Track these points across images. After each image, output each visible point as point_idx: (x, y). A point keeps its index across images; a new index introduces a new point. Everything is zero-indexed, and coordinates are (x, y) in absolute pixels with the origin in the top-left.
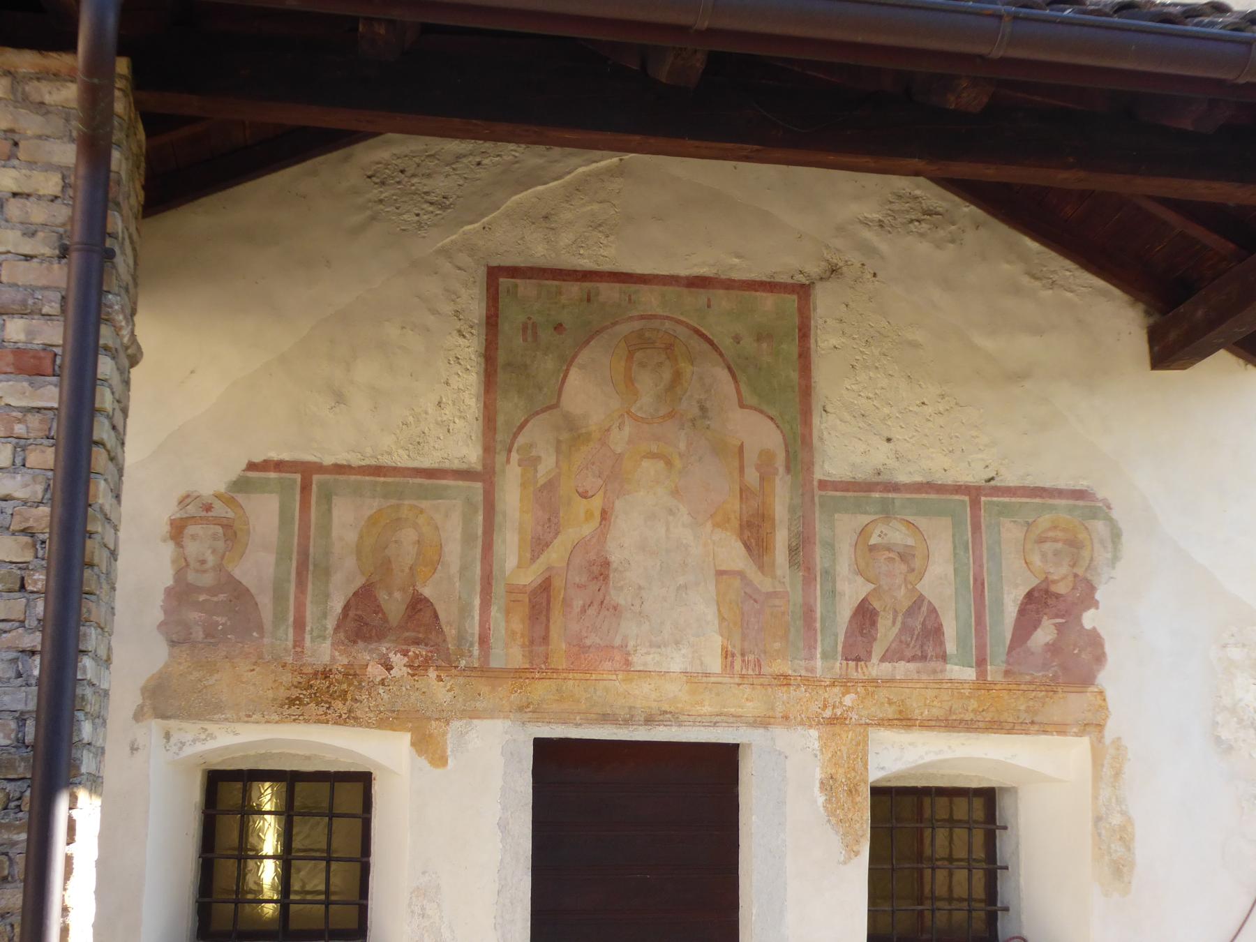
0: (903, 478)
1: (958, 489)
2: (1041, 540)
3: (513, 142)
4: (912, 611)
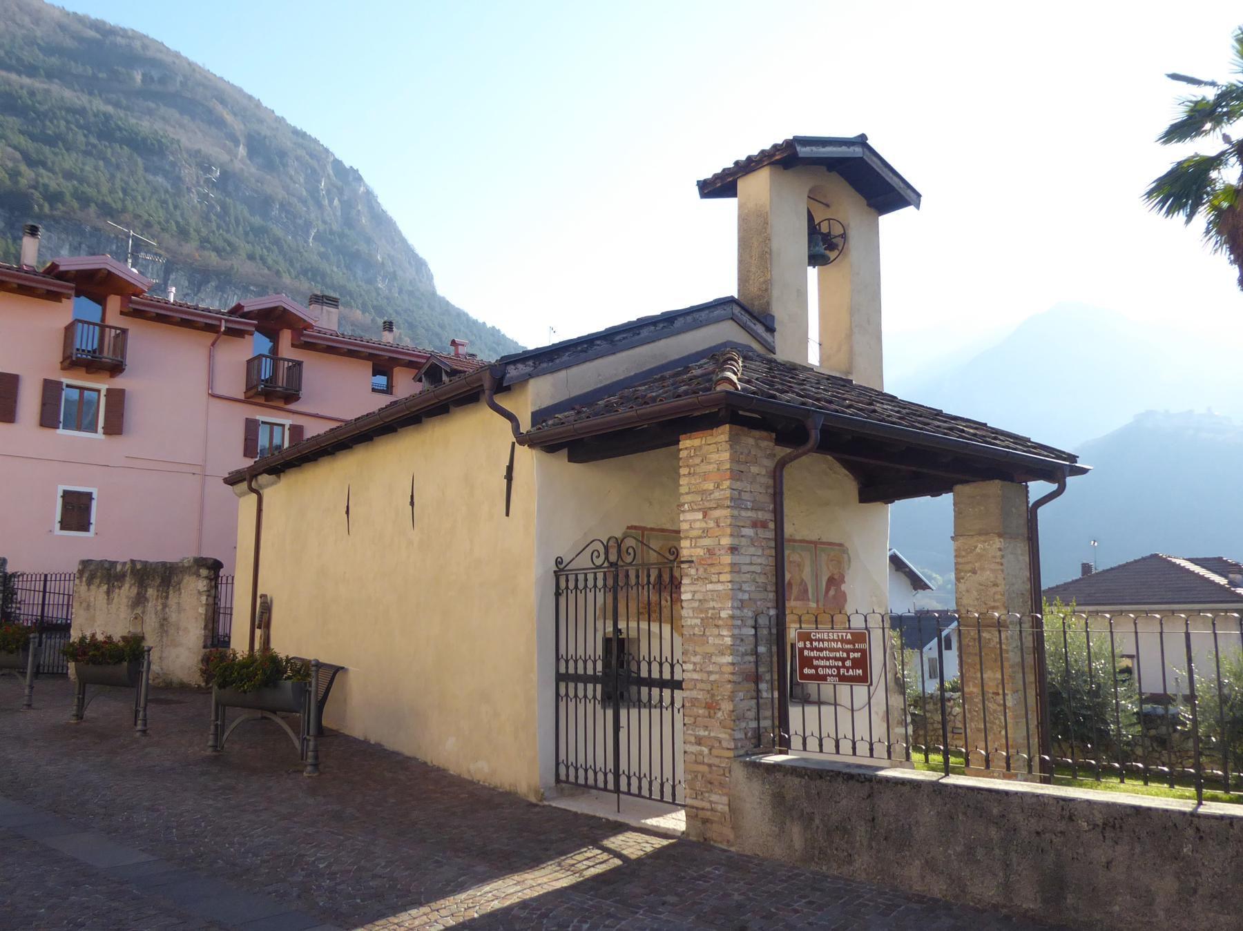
0: (798, 537)
1: (811, 542)
2: (832, 560)
3: (287, 124)
4: (801, 583)
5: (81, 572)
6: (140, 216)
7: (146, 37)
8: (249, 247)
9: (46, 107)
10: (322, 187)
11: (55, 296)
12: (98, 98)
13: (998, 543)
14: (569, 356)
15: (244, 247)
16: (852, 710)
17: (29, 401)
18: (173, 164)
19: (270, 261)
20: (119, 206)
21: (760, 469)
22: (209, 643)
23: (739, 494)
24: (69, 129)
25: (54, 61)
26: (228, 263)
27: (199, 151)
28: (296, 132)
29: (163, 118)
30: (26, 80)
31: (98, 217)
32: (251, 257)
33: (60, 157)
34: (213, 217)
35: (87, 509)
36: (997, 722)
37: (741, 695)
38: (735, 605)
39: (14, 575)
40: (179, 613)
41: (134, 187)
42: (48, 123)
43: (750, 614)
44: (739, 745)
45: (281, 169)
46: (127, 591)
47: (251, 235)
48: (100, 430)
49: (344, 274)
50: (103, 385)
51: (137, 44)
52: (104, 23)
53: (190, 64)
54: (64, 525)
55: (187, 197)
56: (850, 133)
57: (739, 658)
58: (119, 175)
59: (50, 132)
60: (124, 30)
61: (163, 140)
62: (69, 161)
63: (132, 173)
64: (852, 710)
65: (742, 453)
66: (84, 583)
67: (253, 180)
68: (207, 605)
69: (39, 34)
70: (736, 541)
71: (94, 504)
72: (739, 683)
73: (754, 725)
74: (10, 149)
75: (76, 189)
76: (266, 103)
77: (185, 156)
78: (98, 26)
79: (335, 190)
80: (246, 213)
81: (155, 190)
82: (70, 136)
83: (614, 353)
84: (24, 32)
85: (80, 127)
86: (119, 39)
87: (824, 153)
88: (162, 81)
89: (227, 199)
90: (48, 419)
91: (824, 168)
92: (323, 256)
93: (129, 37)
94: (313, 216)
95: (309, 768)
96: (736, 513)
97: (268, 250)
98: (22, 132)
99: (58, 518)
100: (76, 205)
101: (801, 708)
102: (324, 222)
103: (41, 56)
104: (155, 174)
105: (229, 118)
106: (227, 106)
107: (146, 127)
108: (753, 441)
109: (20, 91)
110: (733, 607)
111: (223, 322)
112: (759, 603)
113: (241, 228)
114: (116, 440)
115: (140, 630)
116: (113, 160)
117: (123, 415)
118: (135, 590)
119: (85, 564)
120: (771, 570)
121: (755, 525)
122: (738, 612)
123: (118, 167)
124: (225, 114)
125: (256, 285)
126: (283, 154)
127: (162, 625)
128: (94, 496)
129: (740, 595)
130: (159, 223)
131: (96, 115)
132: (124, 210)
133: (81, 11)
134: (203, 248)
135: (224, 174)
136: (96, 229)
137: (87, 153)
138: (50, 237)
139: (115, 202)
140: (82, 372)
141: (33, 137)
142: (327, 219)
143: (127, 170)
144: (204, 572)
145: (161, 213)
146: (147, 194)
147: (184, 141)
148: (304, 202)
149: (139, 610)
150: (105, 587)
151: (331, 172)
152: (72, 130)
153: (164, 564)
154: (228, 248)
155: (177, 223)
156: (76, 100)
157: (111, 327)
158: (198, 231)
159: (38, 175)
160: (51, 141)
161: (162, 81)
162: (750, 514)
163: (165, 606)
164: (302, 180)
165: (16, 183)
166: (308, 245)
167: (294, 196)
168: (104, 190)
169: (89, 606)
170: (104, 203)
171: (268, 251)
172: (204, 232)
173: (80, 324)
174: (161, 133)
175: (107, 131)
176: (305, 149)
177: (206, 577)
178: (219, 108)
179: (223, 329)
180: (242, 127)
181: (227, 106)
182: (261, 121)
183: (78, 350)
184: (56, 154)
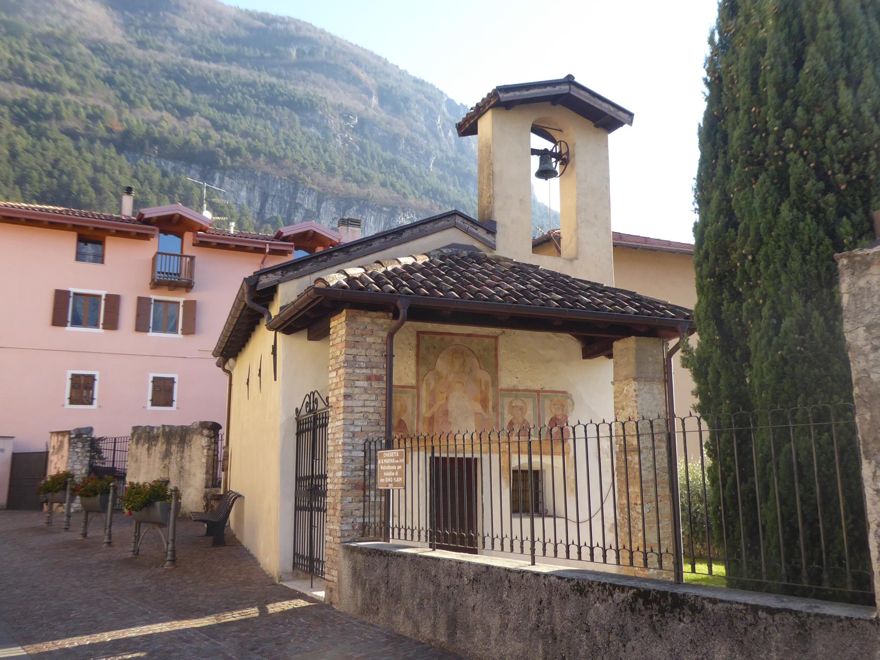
5: (133, 435)
6: (297, 160)
7: (299, 21)
8: (382, 177)
9: (228, 84)
10: (439, 122)
11: (145, 237)
12: (265, 72)
13: (634, 385)
14: (311, 265)
15: (378, 177)
16: (578, 523)
17: (128, 313)
18: (322, 117)
19: (398, 186)
20: (282, 154)
21: (376, 340)
22: (210, 484)
23: (354, 357)
24: (244, 98)
25: (233, 48)
26: (366, 191)
27: (341, 105)
28: (416, 81)
29: (314, 83)
30: (213, 66)
31: (266, 164)
32: (383, 185)
33: (238, 121)
34: (354, 156)
35: (170, 391)
36: (636, 526)
37: (350, 499)
38: (347, 435)
39: (100, 439)
40: (190, 463)
41: (294, 138)
42: (229, 96)
43: (361, 442)
44: (346, 534)
45: (406, 112)
46: (160, 448)
47: (384, 167)
48: (180, 332)
49: (459, 191)
50: (180, 298)
51: (293, 27)
52: (267, 14)
53: (332, 37)
54: (155, 403)
55: (334, 142)
56: (561, 76)
57: (349, 473)
58: (282, 130)
59: (231, 103)
60: (283, 18)
61: (314, 100)
62: (245, 123)
63: (292, 127)
64: (578, 523)
65: (357, 329)
66: (134, 444)
67: (384, 123)
68: (208, 456)
69: (221, 29)
70: (349, 391)
71: (176, 386)
72: (348, 491)
73: (361, 520)
74: (202, 120)
75: (249, 144)
76: (392, 60)
77: (330, 109)
78: (265, 18)
79: (449, 124)
80: (379, 150)
81: (309, 139)
82: (245, 105)
83: (350, 261)
84: (211, 29)
85: (252, 96)
86: (279, 26)
87: (528, 95)
88: (311, 53)
89: (365, 140)
90: (141, 326)
91: (548, 104)
92: (442, 178)
93: (286, 23)
94: (432, 147)
95: (168, 563)
96: (350, 371)
97: (398, 177)
98: (211, 105)
99: (150, 397)
100: (250, 156)
101: (519, 520)
102: (442, 151)
103: (223, 46)
104: (309, 127)
105: (363, 76)
106: (361, 67)
107: (300, 90)
108: (365, 320)
109: (208, 75)
110: (344, 437)
111: (268, 245)
112: (370, 434)
113: (376, 162)
114: (190, 338)
115: (166, 476)
116: (278, 119)
117: (195, 319)
118: (164, 447)
119: (135, 429)
120: (382, 410)
121: (369, 378)
122: (349, 441)
123: (281, 124)
124: (360, 73)
125: (387, 207)
126: (406, 100)
127: (180, 472)
128: (176, 380)
129: (352, 429)
130: (312, 164)
131: (263, 86)
132: (286, 157)
133: (250, 8)
134: (345, 180)
135: (362, 121)
136: (265, 174)
137: (258, 116)
138: (232, 183)
139: (279, 152)
140: (165, 290)
141: (219, 109)
142: (444, 148)
143: (288, 126)
144: (206, 432)
145: (315, 156)
146: (303, 143)
147: (330, 98)
148: (425, 136)
149: (166, 462)
150: (146, 446)
151: (445, 110)
152: (247, 99)
153: (182, 427)
154: (365, 179)
155: (326, 163)
156: (249, 76)
157: (186, 256)
158: (341, 168)
159: (222, 136)
160: (231, 110)
161: (311, 53)
162: (364, 371)
163: (182, 458)
164: (422, 119)
165: (206, 144)
166: (429, 171)
167: (416, 132)
168: (271, 143)
169: (137, 459)
170: (270, 153)
171: (398, 179)
172: (347, 168)
173: (160, 256)
174: (312, 94)
175: (272, 97)
176: (423, 93)
177: (207, 436)
178: (356, 70)
179: (267, 250)
180: (374, 82)
181: (361, 67)
182: (388, 75)
183: (159, 272)
184: (235, 119)
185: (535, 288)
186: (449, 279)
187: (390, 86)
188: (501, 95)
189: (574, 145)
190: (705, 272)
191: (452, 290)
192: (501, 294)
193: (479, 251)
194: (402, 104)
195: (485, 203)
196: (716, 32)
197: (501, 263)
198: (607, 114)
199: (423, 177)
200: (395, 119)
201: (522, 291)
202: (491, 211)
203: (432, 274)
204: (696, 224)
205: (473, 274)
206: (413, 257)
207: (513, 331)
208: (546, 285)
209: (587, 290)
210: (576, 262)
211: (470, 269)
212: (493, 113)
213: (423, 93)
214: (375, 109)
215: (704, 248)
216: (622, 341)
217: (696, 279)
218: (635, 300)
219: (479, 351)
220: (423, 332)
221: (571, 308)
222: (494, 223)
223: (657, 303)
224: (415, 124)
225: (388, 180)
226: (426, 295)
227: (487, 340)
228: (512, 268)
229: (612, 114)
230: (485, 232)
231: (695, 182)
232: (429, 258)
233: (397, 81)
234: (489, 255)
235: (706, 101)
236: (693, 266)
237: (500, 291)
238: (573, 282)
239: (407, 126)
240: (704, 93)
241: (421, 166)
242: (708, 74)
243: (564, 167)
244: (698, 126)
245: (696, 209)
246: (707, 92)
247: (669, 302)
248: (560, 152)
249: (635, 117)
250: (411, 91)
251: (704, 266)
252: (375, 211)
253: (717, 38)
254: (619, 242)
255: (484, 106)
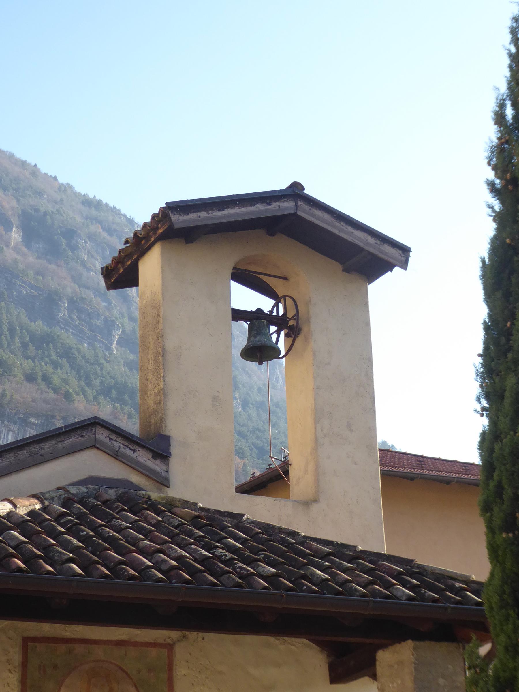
8: (28, 364)
19: (56, 380)
32: (30, 378)
47: (31, 347)
56: (282, 184)
67: (31, 273)
94: (116, 312)
97: (56, 365)
113: (17, 340)
125: (38, 416)
167: (88, 288)
171: (55, 368)
176: (100, 222)
180: (14, 203)
182: (39, 193)
185: (229, 555)
186: (70, 542)
187: (42, 209)
188: (174, 218)
189: (308, 303)
190: (498, 521)
191: (71, 560)
192: (164, 567)
193: (137, 488)
194: (64, 241)
195: (151, 402)
196: (508, 103)
197: (177, 510)
198: (362, 250)
199: (100, 364)
200: (52, 267)
201: (203, 560)
202: (161, 419)
203: (39, 533)
204: (483, 435)
205: (119, 530)
206: (11, 502)
207: (201, 634)
208: (252, 550)
209: (325, 556)
210: (315, 507)
211: (115, 522)
212: (163, 248)
213: (100, 222)
214: (15, 249)
215: (495, 477)
216: (391, 648)
217: (487, 535)
218: (412, 575)
219: (139, 671)
220: (35, 639)
221: (290, 589)
222: (166, 439)
223: (452, 578)
224: (85, 273)
225: (37, 369)
226: (20, 570)
227: (154, 652)
228: (195, 521)
229: (372, 250)
230: (150, 456)
231: (480, 360)
232: (42, 502)
233: (56, 202)
234: (155, 496)
235: (494, 220)
236: (477, 511)
237: (164, 561)
238: (302, 544)
239: (73, 277)
240: (491, 207)
241: (97, 344)
242: (497, 176)
243: (291, 340)
244: (480, 264)
245: (484, 409)
246: (497, 206)
247: (474, 577)
248: (285, 314)
249: (411, 254)
250: (78, 219)
251: (496, 509)
252: (15, 423)
253: (509, 112)
254: (418, 471)
255: (147, 237)
